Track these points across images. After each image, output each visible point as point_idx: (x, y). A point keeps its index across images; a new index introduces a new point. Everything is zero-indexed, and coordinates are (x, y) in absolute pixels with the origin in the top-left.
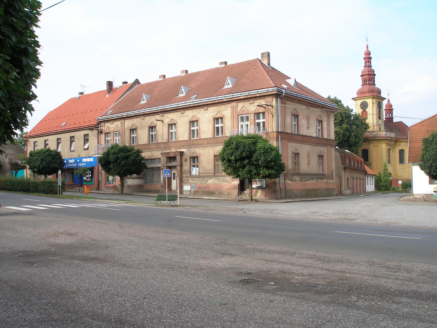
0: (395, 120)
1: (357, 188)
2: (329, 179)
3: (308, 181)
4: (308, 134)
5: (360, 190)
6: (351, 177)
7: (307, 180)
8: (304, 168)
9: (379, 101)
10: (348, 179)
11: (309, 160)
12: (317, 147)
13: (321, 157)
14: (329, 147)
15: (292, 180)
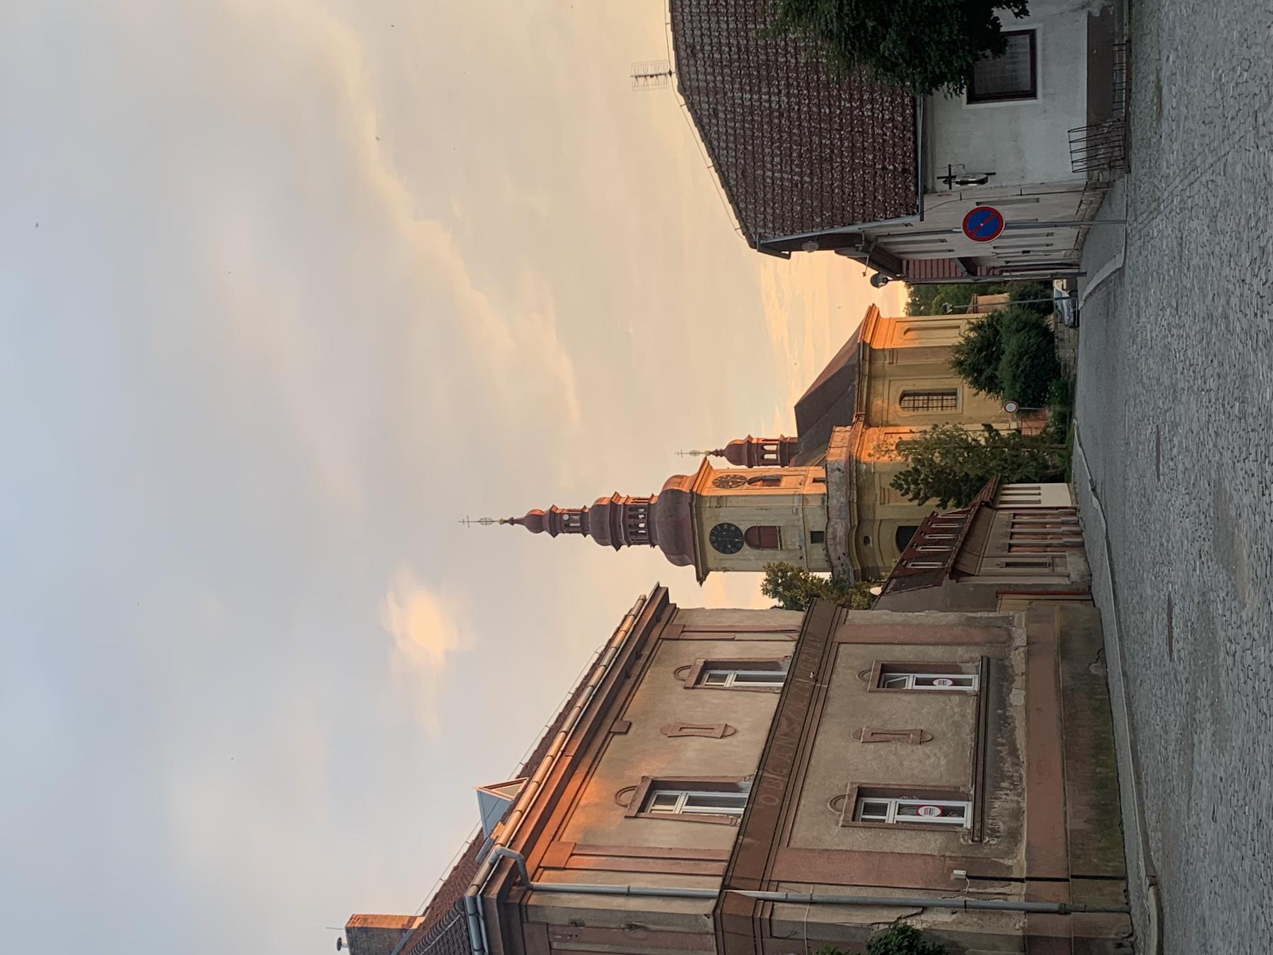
0: (791, 432)
2: (1010, 638)
3: (1021, 743)
4: (762, 736)
6: (1006, 553)
7: (1014, 752)
8: (943, 762)
10: (1008, 565)
11: (902, 735)
12: (831, 693)
13: (887, 676)
14: (841, 635)
15: (1014, 835)
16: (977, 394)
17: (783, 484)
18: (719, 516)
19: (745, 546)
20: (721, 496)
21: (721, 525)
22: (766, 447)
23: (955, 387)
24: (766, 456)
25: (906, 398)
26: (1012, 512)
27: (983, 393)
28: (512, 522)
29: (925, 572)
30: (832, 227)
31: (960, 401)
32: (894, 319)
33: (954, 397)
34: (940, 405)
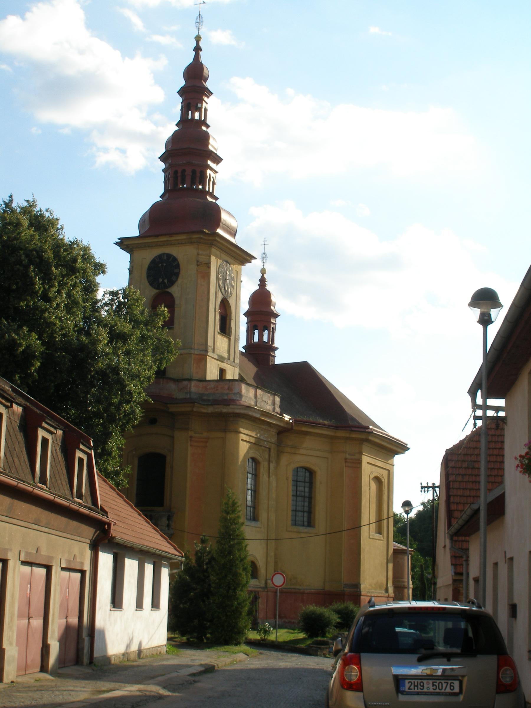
19: (154, 291)
22: (266, 332)
24: (256, 332)
25: (307, 474)
28: (197, 49)
30: (332, 677)
31: (302, 529)
32: (390, 474)
33: (306, 523)
34: (298, 508)
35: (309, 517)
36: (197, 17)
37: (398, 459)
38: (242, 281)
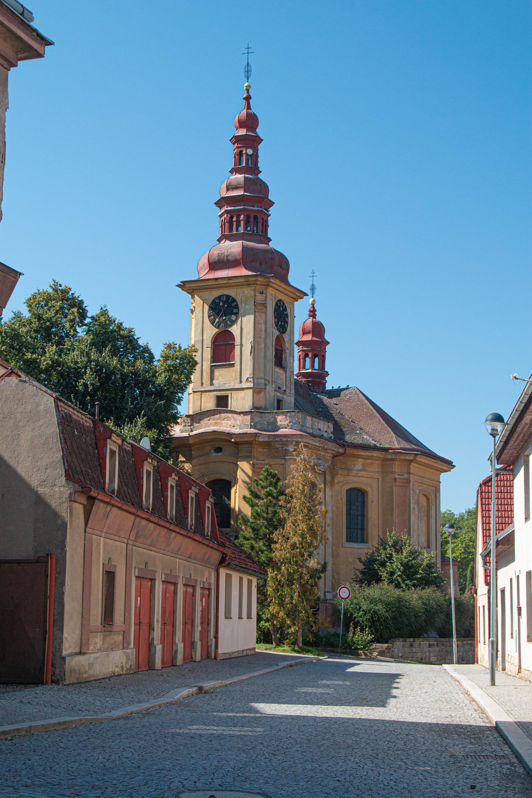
1: (192, 632)
5: (190, 645)
9: (280, 301)
16: (360, 561)
17: (277, 370)
18: (245, 304)
19: (215, 331)
20: (266, 307)
21: (237, 307)
23: (370, 542)
25: (360, 494)
26: (213, 587)
27: (361, 567)
29: (100, 465)
33: (359, 540)
35: (363, 535)
36: (246, 66)
37: (443, 477)
38: (295, 317)
